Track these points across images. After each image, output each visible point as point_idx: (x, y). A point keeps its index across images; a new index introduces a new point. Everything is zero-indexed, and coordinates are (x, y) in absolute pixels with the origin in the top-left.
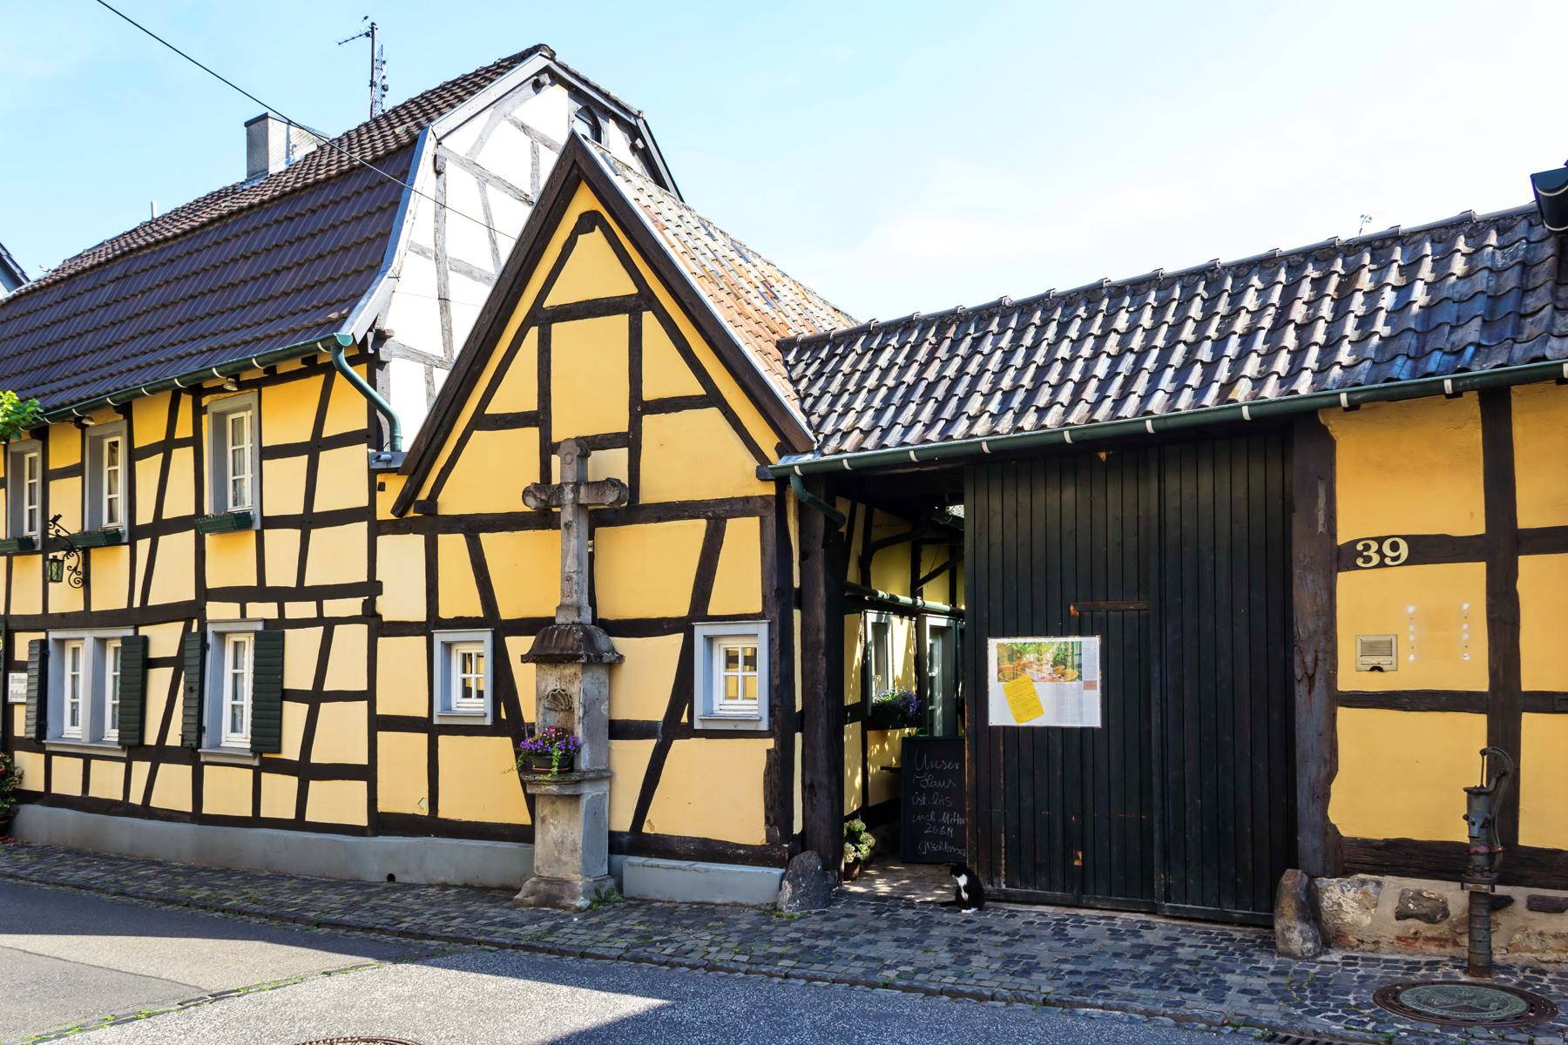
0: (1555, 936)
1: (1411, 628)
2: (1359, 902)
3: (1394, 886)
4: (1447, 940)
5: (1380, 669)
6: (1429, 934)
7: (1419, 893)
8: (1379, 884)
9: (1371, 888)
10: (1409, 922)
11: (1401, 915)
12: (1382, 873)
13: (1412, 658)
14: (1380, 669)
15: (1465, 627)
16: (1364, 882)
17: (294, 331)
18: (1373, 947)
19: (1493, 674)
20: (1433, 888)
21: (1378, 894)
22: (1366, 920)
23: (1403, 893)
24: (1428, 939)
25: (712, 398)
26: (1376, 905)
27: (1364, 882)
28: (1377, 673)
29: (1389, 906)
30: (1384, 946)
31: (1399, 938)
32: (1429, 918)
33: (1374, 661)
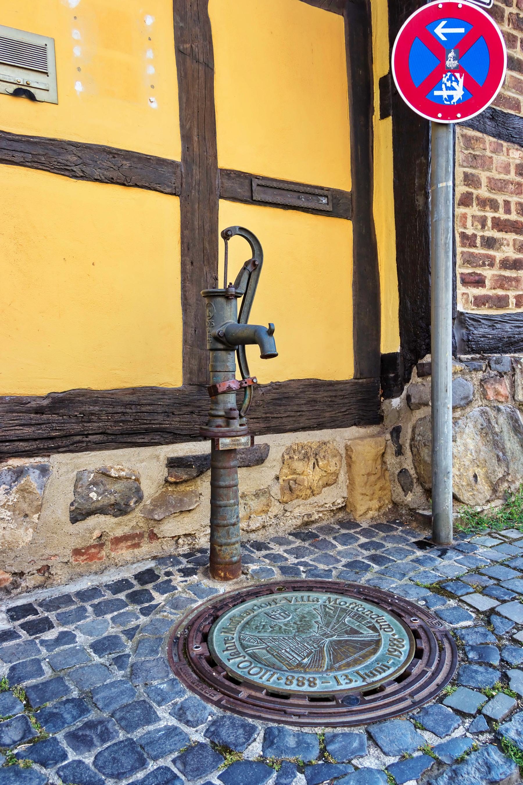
0: (257, 495)
1: (76, 34)
2: (13, 508)
3: (66, 467)
4: (141, 536)
5: (32, 97)
6: (119, 533)
7: (105, 474)
8: (44, 470)
9: (33, 479)
10: (92, 521)
11: (78, 515)
12: (47, 452)
13: (149, 21)
14: (32, 97)
15: (150, 54)
16: (20, 473)
17: (445, 244)
18: (39, 578)
19: (186, 138)
20: (121, 461)
21: (43, 487)
22: (25, 536)
23: (78, 479)
24: (117, 541)
25: (356, 207)
26: (39, 509)
27: (20, 473)
28: (23, 103)
29: (60, 497)
30: (59, 573)
31: (77, 552)
32: (120, 509)
33: (22, 77)
